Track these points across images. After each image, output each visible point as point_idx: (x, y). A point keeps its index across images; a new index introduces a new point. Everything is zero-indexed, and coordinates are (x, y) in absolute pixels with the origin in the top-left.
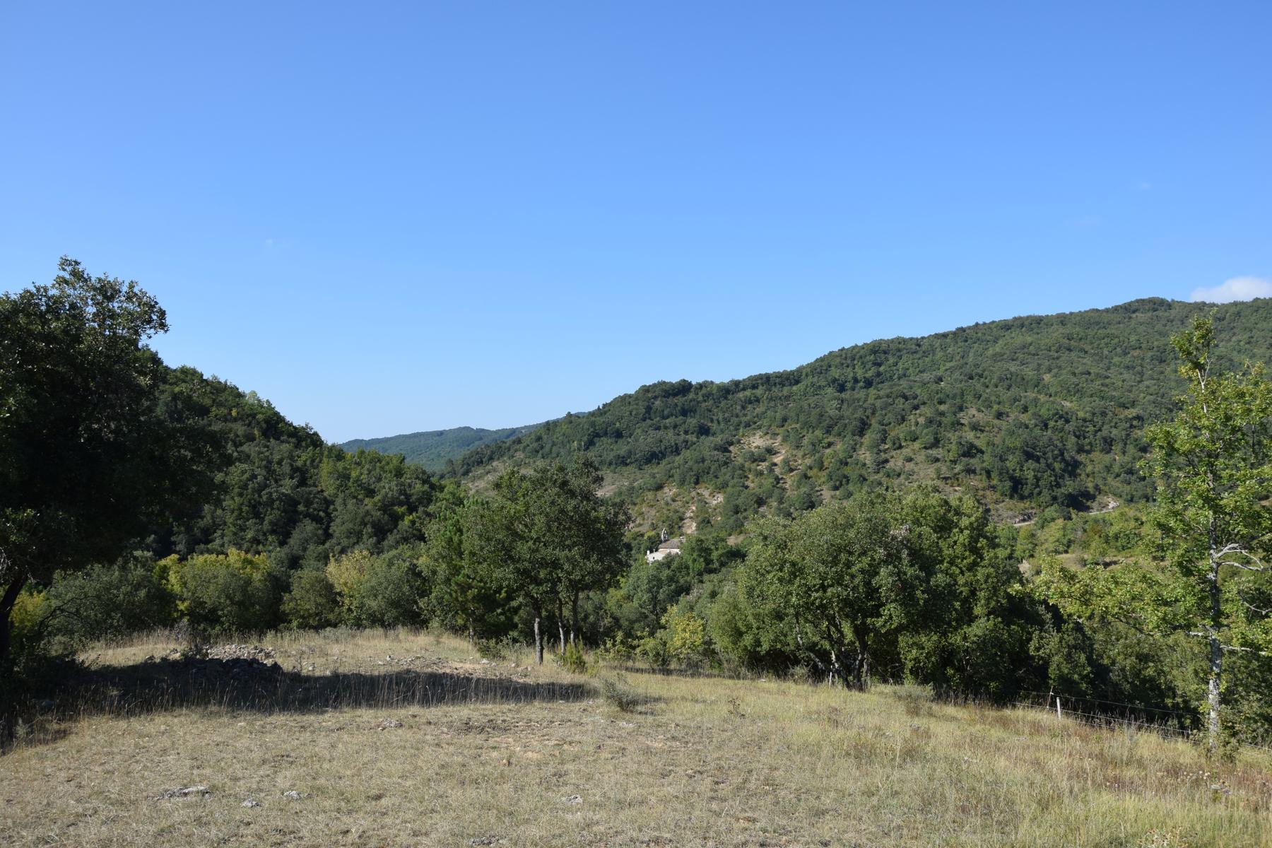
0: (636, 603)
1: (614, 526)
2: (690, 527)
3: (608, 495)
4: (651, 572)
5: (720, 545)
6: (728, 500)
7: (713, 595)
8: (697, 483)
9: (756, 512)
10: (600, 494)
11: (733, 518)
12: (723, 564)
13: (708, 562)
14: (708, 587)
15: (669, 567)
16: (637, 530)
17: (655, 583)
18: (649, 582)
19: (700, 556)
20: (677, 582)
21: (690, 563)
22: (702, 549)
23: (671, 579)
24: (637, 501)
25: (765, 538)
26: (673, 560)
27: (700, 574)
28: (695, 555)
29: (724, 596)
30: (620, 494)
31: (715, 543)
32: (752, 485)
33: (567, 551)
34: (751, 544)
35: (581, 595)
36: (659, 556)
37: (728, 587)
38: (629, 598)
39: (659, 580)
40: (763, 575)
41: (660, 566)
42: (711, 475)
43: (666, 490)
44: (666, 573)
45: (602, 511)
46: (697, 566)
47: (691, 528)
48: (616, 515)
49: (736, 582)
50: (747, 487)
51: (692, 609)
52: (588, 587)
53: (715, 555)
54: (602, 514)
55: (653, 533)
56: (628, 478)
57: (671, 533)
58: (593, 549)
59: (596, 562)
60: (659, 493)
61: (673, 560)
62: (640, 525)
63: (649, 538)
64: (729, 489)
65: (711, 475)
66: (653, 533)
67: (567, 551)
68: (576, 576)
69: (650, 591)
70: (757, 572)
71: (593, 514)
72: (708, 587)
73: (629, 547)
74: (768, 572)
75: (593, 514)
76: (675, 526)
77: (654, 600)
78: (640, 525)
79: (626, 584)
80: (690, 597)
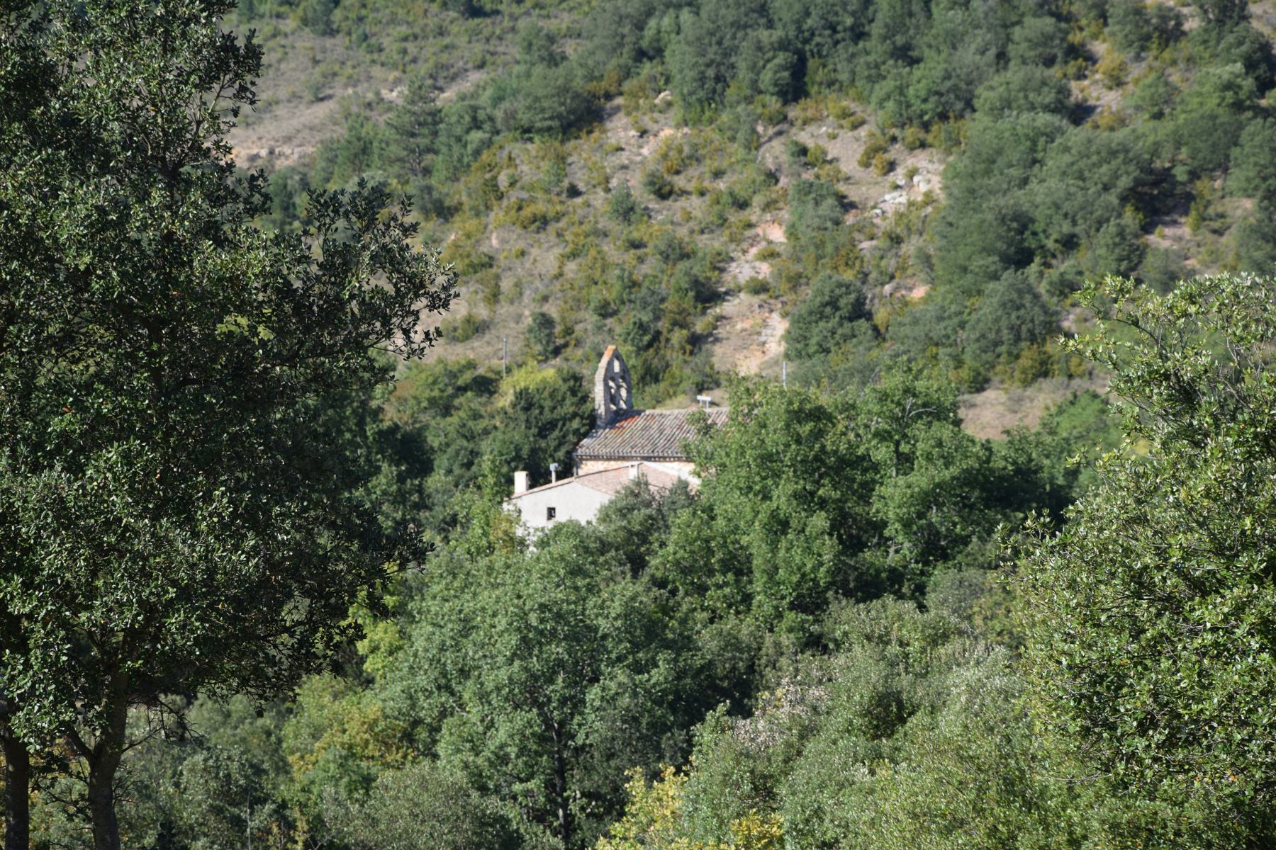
0: (450, 765)
1: (330, 323)
2: (753, 337)
3: (290, 157)
4: (537, 591)
5: (923, 437)
6: (968, 192)
7: (888, 715)
8: (794, 90)
9: (1131, 262)
10: (245, 148)
11: (998, 290)
12: (936, 549)
13: (855, 533)
14: (857, 672)
15: (637, 564)
16: (456, 354)
17: (563, 651)
18: (526, 646)
19: (806, 499)
20: (684, 643)
21: (754, 540)
22: (822, 464)
23: (649, 632)
24: (461, 192)
25: (1186, 396)
26: (657, 522)
27: (810, 602)
28: (782, 495)
29: (949, 723)
30: (361, 152)
31: (897, 430)
32: (1108, 101)
33: (56, 473)
34: (1100, 430)
35: (140, 720)
36: (582, 499)
37: (968, 676)
38: (412, 736)
39: (583, 634)
40: (1171, 604)
41: (586, 554)
42: (875, 47)
43: (619, 130)
44: (618, 596)
45: (255, 251)
46: (792, 553)
47: (757, 344)
48: (340, 262)
49: (1016, 644)
50: (1080, 113)
51: (764, 792)
52: (173, 676)
53: (892, 497)
54: (257, 261)
55: (549, 373)
56: (406, 62)
57: (648, 376)
58: (208, 461)
59: (227, 531)
60: (582, 152)
61: (657, 522)
62: (475, 328)
63: (526, 401)
64: (977, 127)
65: (875, 47)
66: (549, 373)
67: (56, 473)
68: (113, 608)
69: (529, 693)
70: (1140, 584)
71: (209, 260)
72: (857, 672)
73: (411, 453)
74: (1203, 588)
75: (209, 260)
76: (670, 331)
77: (554, 745)
78: (475, 328)
79: (396, 657)
80: (757, 731)
